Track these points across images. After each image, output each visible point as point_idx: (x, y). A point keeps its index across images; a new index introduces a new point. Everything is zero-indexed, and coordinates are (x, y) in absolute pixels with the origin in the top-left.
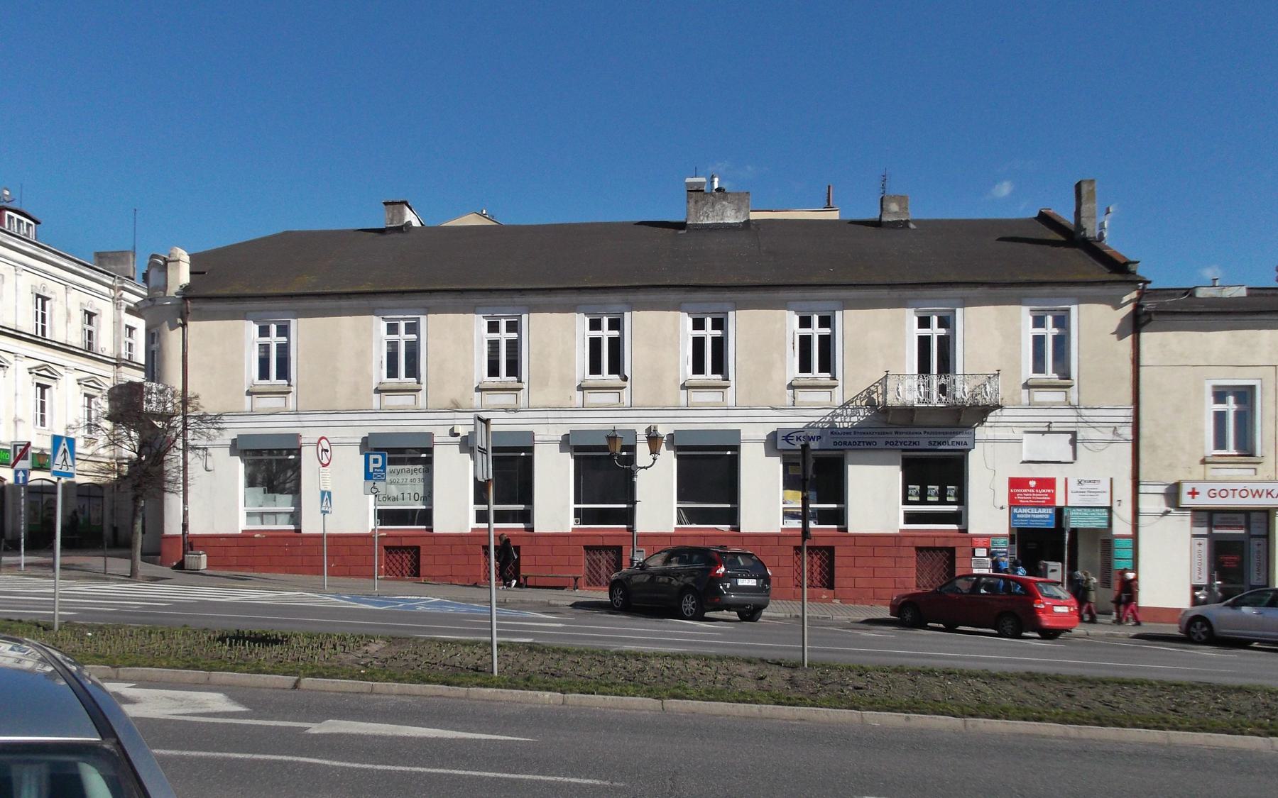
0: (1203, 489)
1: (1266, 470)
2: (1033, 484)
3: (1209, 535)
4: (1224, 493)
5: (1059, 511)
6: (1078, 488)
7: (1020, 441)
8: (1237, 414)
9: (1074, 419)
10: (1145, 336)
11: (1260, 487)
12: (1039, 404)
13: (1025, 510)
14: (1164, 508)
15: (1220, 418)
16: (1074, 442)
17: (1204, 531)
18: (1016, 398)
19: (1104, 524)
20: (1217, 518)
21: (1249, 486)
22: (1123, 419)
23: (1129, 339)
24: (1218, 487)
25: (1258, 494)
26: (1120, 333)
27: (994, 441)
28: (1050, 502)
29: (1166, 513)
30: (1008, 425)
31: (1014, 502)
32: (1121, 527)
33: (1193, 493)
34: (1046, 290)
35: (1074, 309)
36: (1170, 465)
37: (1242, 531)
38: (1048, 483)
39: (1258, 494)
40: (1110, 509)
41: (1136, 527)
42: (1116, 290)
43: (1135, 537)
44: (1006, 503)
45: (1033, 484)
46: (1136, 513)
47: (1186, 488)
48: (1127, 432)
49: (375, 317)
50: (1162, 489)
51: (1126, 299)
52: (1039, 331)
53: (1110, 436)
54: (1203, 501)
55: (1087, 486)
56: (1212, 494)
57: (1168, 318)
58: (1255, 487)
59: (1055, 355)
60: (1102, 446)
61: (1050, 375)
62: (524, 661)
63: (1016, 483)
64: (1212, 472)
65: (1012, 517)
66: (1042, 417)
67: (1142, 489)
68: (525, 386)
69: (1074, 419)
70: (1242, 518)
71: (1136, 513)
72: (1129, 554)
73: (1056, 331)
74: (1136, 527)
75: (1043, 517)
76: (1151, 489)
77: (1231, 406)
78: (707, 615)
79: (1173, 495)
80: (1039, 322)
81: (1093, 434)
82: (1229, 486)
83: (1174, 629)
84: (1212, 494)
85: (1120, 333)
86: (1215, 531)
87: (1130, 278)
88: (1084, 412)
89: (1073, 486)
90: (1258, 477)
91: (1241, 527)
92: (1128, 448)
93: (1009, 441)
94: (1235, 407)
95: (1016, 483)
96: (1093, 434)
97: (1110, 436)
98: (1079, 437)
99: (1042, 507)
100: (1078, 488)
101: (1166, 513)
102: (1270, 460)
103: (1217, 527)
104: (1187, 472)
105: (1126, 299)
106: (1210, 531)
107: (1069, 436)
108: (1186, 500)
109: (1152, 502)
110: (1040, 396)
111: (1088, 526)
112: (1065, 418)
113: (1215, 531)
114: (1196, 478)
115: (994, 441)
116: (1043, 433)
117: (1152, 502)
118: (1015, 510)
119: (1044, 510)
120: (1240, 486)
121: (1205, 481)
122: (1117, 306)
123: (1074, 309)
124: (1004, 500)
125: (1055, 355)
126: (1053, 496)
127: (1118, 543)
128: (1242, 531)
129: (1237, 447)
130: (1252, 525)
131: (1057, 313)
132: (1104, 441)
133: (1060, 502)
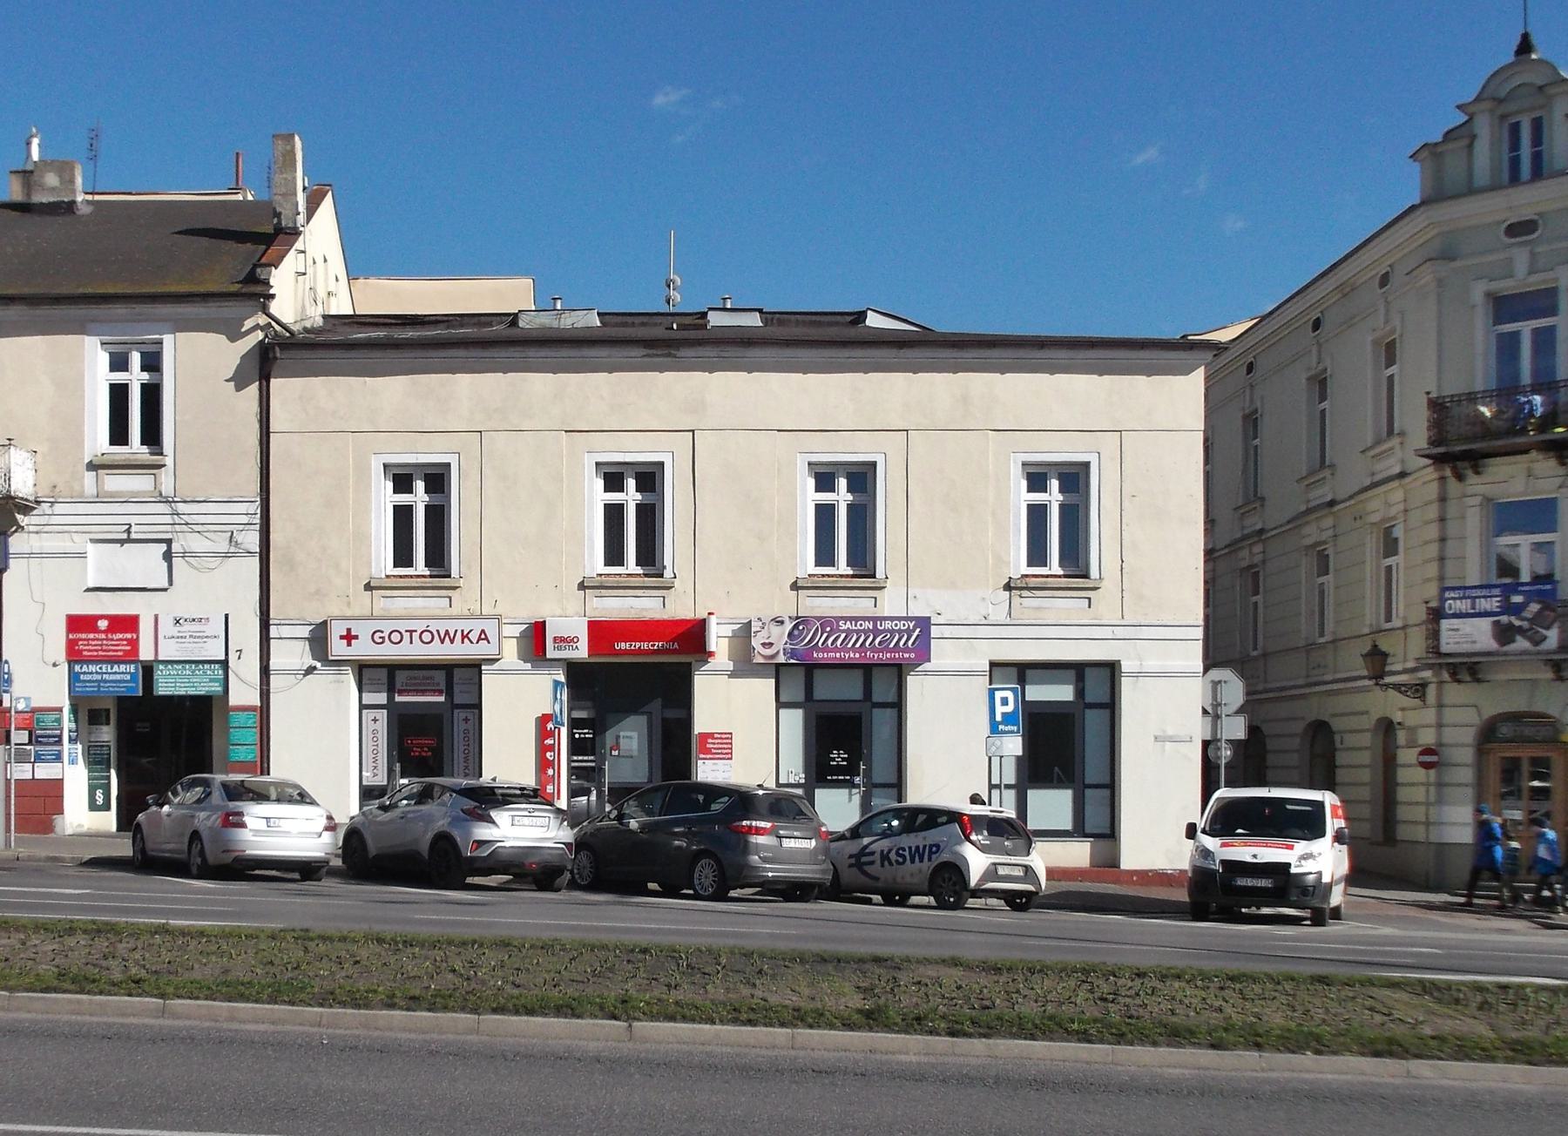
0: (363, 630)
1: (1106, 602)
2: (103, 624)
3: (390, 706)
4: (395, 638)
5: (148, 670)
6: (175, 631)
7: (82, 555)
8: (1063, 508)
9: (168, 519)
10: (276, 383)
11: (452, 626)
12: (112, 495)
13: (92, 668)
14: (309, 661)
15: (825, 514)
16: (168, 556)
17: (382, 698)
18: (77, 487)
19: (217, 688)
20: (401, 677)
21: (434, 626)
22: (245, 519)
23: (253, 389)
24: (387, 627)
25: (447, 637)
26: (239, 380)
27: (42, 555)
28: (131, 655)
29: (311, 670)
30: (63, 530)
31: (74, 655)
32: (243, 693)
33: (349, 637)
34: (120, 310)
35: (168, 339)
36: (317, 592)
37: (442, 699)
38: (128, 624)
39: (447, 637)
40: (225, 664)
41: (265, 694)
42: (229, 310)
43: (264, 711)
44: (61, 655)
45: (103, 624)
46: (265, 671)
47: (337, 630)
48: (252, 540)
49: (87, 338)
50: (305, 632)
51: (248, 324)
52: (120, 377)
53: (223, 546)
54: (364, 649)
55: (187, 627)
56: (377, 638)
57: (305, 354)
58: (442, 626)
59: (139, 417)
60: (215, 562)
61: (136, 446)
62: (340, 975)
63: (78, 624)
64: (382, 603)
65: (73, 678)
66: (114, 517)
67: (273, 632)
68: (169, 461)
69: (168, 519)
70: (440, 677)
71: (265, 671)
72: (253, 736)
73: (145, 376)
74: (265, 694)
75: (121, 677)
76: (286, 631)
77: (1053, 496)
78: (733, 894)
79: (319, 639)
80: (119, 363)
81: (196, 543)
82: (403, 626)
83: (1182, 895)
84: (377, 638)
85: (239, 380)
86: (398, 699)
87: (259, 289)
88: (181, 507)
89: (166, 627)
90: (455, 611)
91: (440, 692)
92: (255, 562)
93: (65, 555)
94: (850, 497)
95: (78, 624)
96: (196, 543)
97: (223, 546)
98: (175, 547)
99: (119, 661)
100: (175, 631)
101: (311, 670)
102: (1109, 586)
103: (401, 693)
104: (340, 602)
105: (248, 324)
106: (391, 698)
107: (164, 547)
108: (338, 648)
109: (290, 654)
110: (116, 482)
111: (192, 692)
112: (151, 519)
113: (398, 699)
114: (357, 612)
115: (42, 555)
116: (122, 542)
117: (290, 654)
118: (77, 668)
119: (123, 668)
120: (419, 626)
121: (371, 618)
122: (235, 335)
123: (168, 339)
124: (59, 651)
125: (139, 417)
126: (134, 644)
127: (237, 719)
128: (442, 699)
129: (429, 563)
130: (456, 689)
131: (146, 348)
132: (216, 555)
133: (146, 654)
